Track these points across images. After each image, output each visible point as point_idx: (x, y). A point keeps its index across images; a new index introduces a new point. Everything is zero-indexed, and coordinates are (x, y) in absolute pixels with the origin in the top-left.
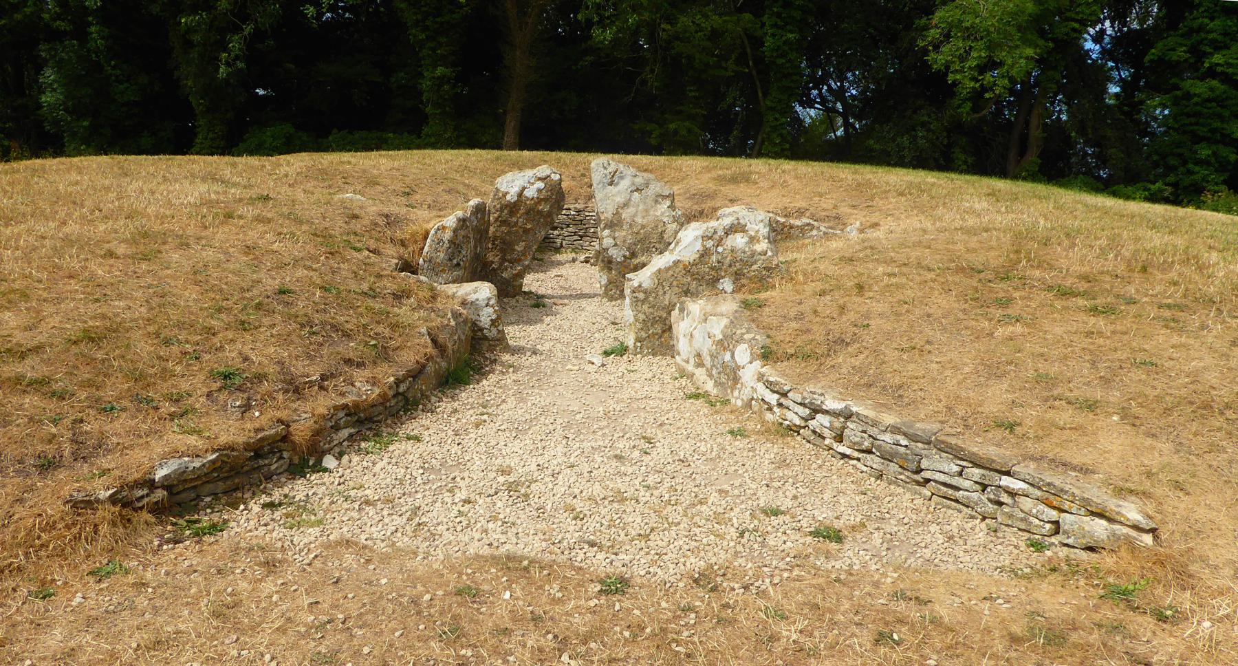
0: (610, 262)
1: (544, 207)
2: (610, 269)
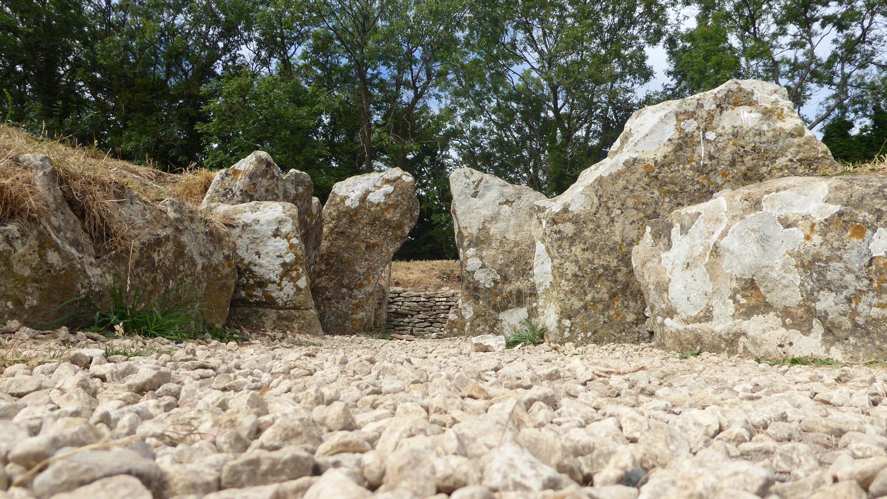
0: (476, 289)
2: (477, 299)
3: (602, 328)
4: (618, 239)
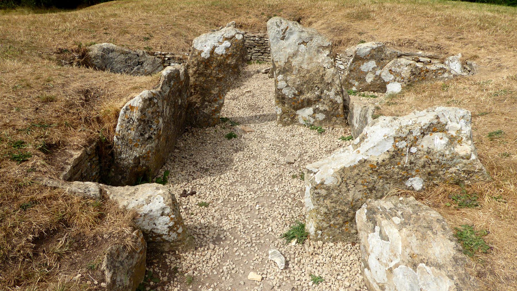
1: (232, 61)
2: (284, 103)
3: (338, 235)
4: (350, 199)
